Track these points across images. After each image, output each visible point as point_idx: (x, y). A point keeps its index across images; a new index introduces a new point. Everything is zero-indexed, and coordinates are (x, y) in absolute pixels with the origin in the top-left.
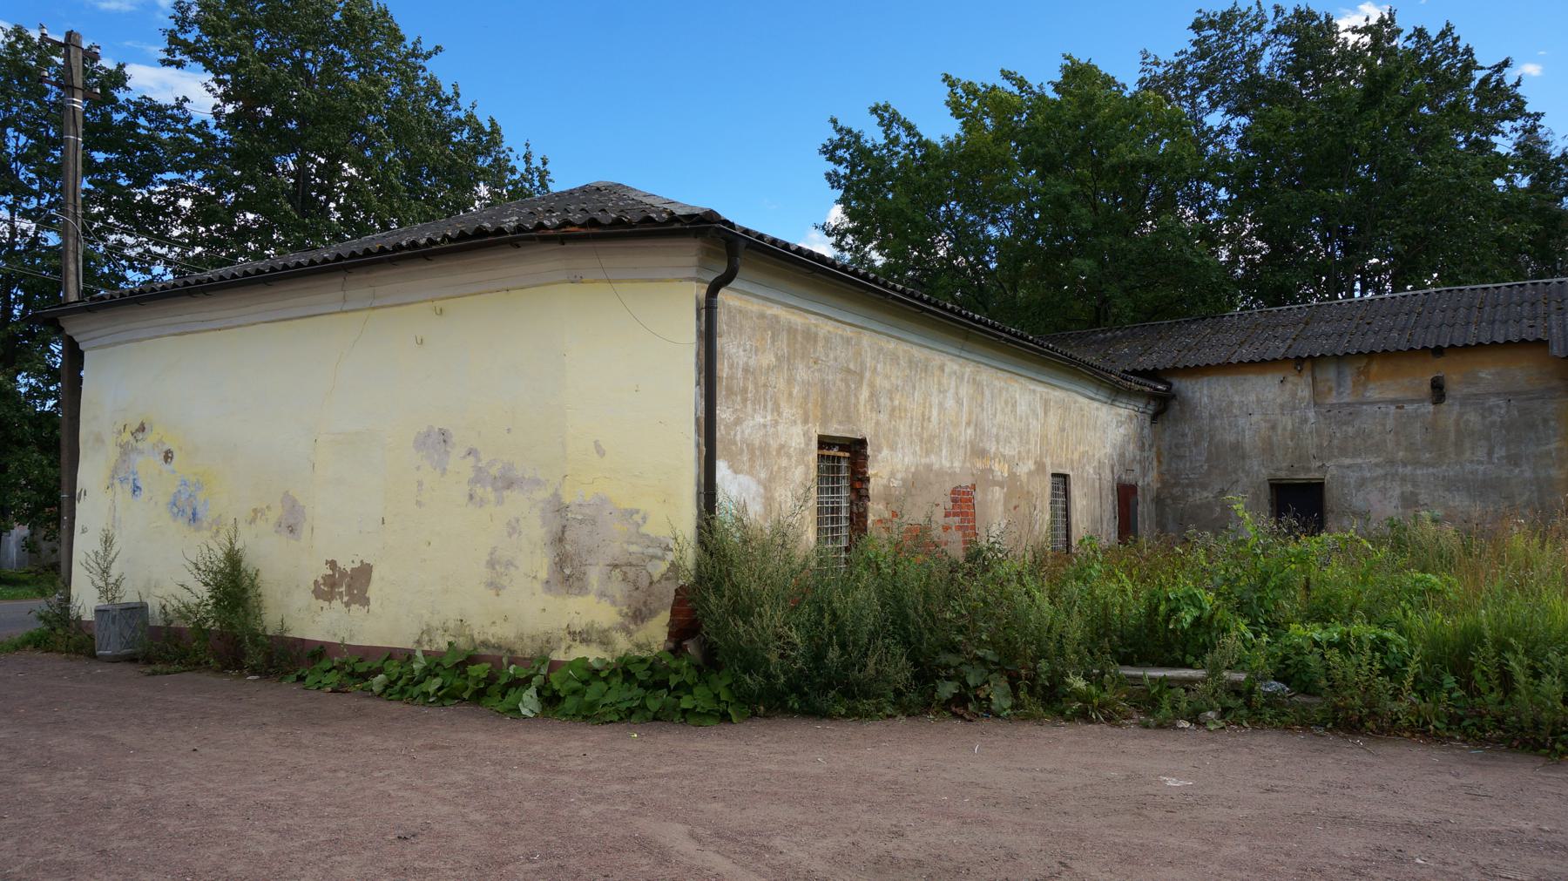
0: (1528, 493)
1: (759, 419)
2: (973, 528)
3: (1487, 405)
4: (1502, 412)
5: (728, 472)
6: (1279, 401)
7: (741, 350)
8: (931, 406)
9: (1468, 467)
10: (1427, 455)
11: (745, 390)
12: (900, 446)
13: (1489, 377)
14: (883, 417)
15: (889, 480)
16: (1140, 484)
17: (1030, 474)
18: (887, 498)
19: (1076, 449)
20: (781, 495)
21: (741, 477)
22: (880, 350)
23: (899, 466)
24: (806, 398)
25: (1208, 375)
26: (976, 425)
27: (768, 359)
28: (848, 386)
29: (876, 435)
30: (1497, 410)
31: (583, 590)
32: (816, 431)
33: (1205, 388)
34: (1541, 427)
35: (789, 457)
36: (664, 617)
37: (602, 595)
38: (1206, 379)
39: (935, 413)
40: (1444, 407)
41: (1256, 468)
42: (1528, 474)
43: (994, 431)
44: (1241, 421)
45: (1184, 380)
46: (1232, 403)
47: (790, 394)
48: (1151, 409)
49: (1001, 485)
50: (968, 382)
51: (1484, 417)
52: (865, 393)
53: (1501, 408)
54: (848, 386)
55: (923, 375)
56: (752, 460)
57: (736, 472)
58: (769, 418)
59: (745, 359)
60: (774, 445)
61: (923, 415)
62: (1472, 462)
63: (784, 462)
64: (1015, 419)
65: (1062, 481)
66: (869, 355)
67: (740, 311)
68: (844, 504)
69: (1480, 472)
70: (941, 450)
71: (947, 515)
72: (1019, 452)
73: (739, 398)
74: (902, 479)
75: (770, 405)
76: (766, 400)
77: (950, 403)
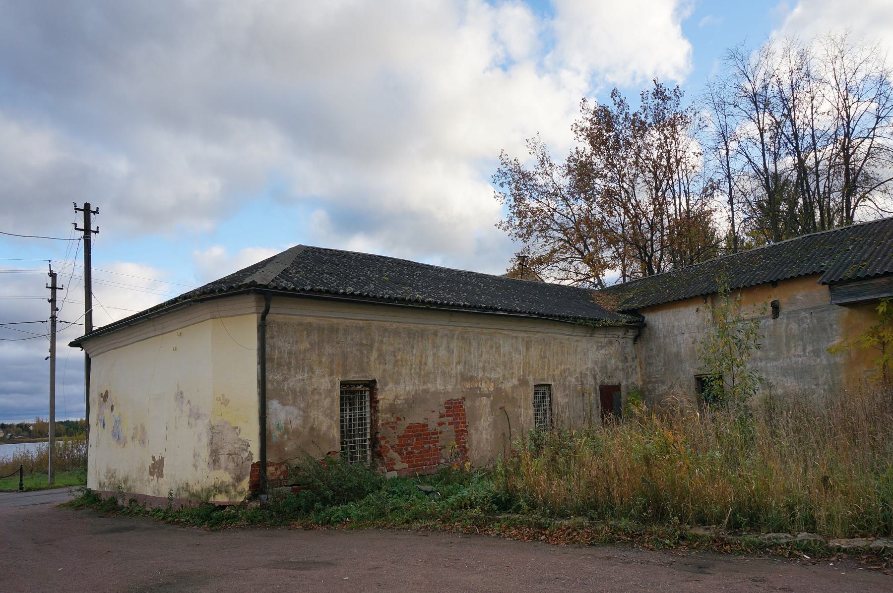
0: (826, 375)
1: (299, 377)
2: (464, 422)
3: (800, 318)
4: (808, 321)
5: (278, 405)
6: (696, 324)
7: (286, 343)
8: (427, 356)
9: (793, 359)
10: (772, 353)
11: (290, 363)
12: (402, 381)
13: (802, 298)
14: (389, 367)
15: (394, 400)
16: (624, 383)
17: (514, 387)
18: (392, 409)
19: (557, 368)
20: (314, 415)
21: (287, 408)
22: (386, 330)
23: (402, 393)
24: (331, 362)
25: (661, 310)
26: (465, 363)
27: (305, 345)
28: (361, 352)
29: (384, 377)
30: (805, 320)
31: (219, 467)
32: (338, 379)
33: (660, 318)
34: (829, 330)
35: (320, 394)
36: (248, 479)
37: (226, 469)
38: (661, 312)
39: (430, 359)
40: (778, 320)
41: (688, 368)
42: (824, 362)
43: (481, 365)
44: (679, 338)
45: (650, 314)
46: (673, 327)
47: (320, 362)
48: (631, 334)
49: (488, 396)
50: (458, 339)
51: (799, 326)
52: (375, 355)
53: (807, 319)
54: (361, 352)
55: (420, 339)
56: (295, 398)
57: (284, 405)
58: (306, 376)
59: (289, 348)
60: (309, 389)
61: (420, 362)
62: (795, 356)
63: (317, 397)
64: (500, 356)
65: (543, 391)
66: (377, 335)
67: (286, 324)
68: (368, 415)
69: (800, 363)
70: (436, 380)
71: (442, 416)
72: (504, 375)
73: (286, 367)
74: (404, 399)
75: (306, 369)
76: (304, 367)
77: (442, 352)
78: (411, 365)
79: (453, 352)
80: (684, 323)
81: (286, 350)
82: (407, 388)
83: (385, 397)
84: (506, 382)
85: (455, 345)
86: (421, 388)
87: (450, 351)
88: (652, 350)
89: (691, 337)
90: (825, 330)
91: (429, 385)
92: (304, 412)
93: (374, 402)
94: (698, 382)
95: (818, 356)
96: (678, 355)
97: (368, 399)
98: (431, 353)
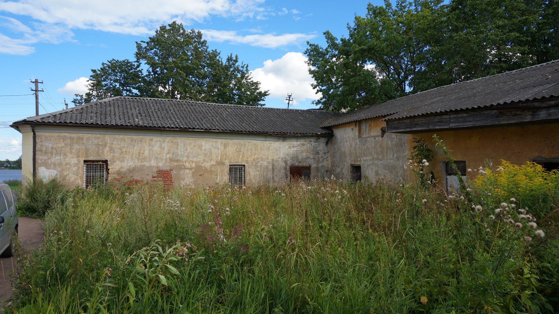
8: (144, 150)
9: (389, 161)
35: (71, 165)
49: (191, 169)
60: (64, 163)
78: (133, 154)
79: (164, 148)
80: (347, 136)
81: (50, 147)
82: (129, 164)
83: (113, 168)
84: (205, 163)
85: (166, 145)
86: (139, 164)
87: (162, 148)
88: (335, 149)
89: (350, 144)
90: (402, 146)
91: (146, 163)
92: (60, 172)
93: (107, 170)
94: (353, 170)
95: (399, 160)
96: (345, 152)
97: (105, 167)
98: (148, 149)
